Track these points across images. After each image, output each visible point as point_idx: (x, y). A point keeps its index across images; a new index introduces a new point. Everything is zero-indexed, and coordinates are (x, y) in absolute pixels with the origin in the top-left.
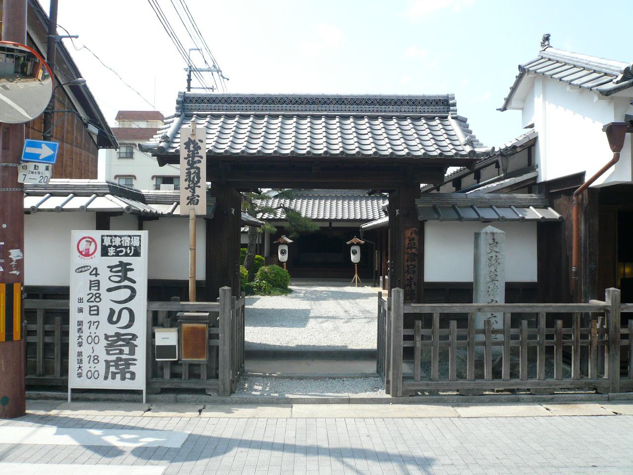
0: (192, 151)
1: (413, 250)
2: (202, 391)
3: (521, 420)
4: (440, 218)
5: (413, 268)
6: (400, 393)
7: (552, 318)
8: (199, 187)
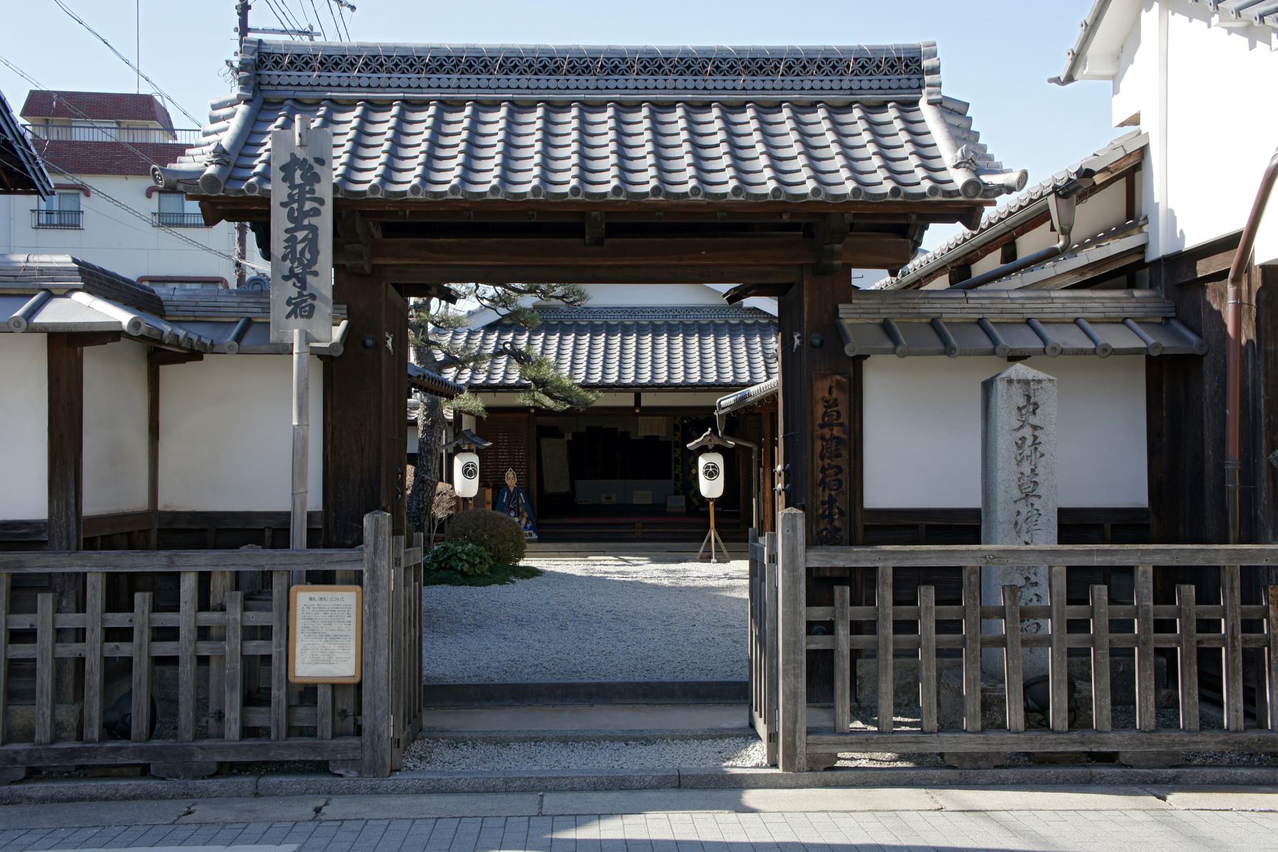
0: (299, 186)
1: (836, 431)
2: (322, 768)
3: (1090, 816)
4: (899, 349)
5: (836, 474)
6: (801, 761)
7: (1167, 579)
8: (316, 274)
